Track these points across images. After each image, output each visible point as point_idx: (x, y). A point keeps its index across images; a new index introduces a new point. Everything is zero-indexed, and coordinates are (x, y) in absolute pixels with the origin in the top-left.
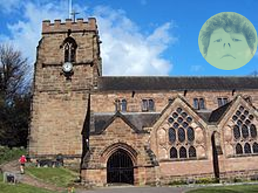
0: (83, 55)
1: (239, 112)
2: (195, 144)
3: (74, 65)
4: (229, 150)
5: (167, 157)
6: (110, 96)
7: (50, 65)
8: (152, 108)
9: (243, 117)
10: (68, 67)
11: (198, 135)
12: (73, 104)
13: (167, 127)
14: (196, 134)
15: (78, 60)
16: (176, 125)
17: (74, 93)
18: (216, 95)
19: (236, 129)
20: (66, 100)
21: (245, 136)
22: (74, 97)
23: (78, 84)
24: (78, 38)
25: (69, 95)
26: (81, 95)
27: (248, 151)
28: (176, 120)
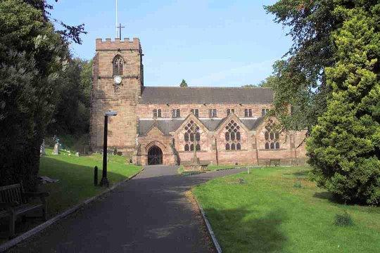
0: (130, 69)
1: (230, 124)
2: (225, 141)
3: (123, 78)
4: (222, 147)
5: (183, 149)
6: (150, 106)
7: (105, 78)
8: (178, 115)
9: (232, 127)
10: (118, 80)
11: (243, 136)
12: (122, 108)
13: (185, 131)
14: (201, 137)
15: (125, 74)
16: (189, 131)
17: (123, 101)
18: (262, 106)
19: (227, 135)
20: (117, 105)
21: (233, 139)
22: (123, 104)
23: (126, 94)
24: (126, 55)
25: (119, 101)
26: (128, 102)
27: (272, 147)
28: (189, 128)
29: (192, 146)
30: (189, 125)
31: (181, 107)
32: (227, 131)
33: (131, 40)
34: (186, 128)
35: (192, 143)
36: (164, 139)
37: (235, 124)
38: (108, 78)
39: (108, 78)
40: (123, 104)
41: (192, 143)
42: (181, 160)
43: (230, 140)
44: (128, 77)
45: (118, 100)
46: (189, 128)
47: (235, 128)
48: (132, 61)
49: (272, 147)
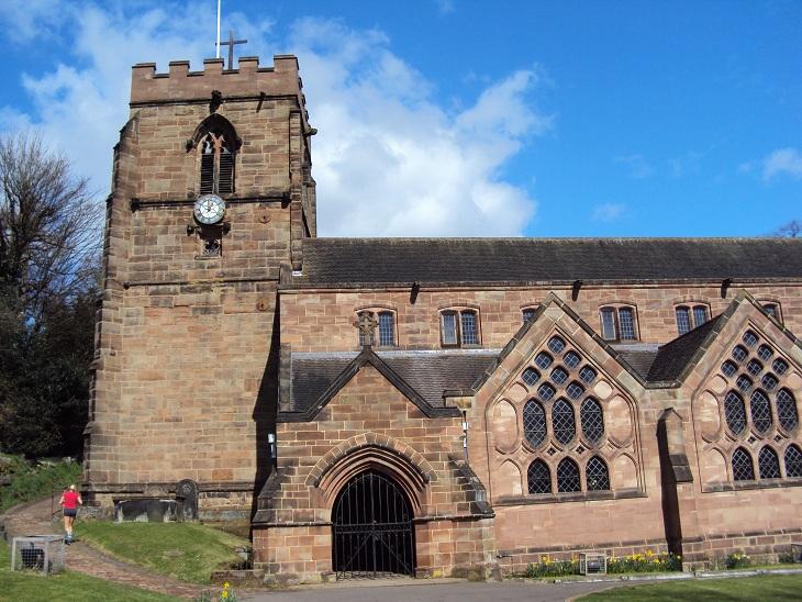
0: (259, 170)
1: (742, 350)
4: (712, 466)
5: (519, 488)
7: (156, 204)
10: (210, 209)
13: (519, 394)
14: (608, 419)
15: (242, 186)
16: (548, 388)
17: (231, 290)
19: (733, 402)
20: (206, 311)
22: (230, 303)
23: (243, 263)
24: (243, 118)
25: (215, 295)
28: (546, 374)
29: (568, 465)
30: (545, 357)
31: (481, 298)
32: (733, 383)
33: (163, 69)
34: (532, 374)
35: (570, 451)
36: (416, 433)
37: (767, 349)
38: (172, 203)
39: (172, 203)
40: (230, 303)
41: (570, 451)
42: (685, 534)
43: (580, 438)
44: (251, 199)
45: (209, 289)
46: (546, 374)
47: (768, 368)
48: (270, 139)
49: (770, 469)
